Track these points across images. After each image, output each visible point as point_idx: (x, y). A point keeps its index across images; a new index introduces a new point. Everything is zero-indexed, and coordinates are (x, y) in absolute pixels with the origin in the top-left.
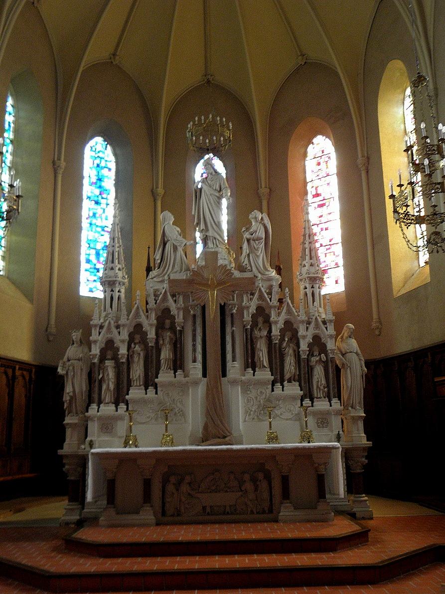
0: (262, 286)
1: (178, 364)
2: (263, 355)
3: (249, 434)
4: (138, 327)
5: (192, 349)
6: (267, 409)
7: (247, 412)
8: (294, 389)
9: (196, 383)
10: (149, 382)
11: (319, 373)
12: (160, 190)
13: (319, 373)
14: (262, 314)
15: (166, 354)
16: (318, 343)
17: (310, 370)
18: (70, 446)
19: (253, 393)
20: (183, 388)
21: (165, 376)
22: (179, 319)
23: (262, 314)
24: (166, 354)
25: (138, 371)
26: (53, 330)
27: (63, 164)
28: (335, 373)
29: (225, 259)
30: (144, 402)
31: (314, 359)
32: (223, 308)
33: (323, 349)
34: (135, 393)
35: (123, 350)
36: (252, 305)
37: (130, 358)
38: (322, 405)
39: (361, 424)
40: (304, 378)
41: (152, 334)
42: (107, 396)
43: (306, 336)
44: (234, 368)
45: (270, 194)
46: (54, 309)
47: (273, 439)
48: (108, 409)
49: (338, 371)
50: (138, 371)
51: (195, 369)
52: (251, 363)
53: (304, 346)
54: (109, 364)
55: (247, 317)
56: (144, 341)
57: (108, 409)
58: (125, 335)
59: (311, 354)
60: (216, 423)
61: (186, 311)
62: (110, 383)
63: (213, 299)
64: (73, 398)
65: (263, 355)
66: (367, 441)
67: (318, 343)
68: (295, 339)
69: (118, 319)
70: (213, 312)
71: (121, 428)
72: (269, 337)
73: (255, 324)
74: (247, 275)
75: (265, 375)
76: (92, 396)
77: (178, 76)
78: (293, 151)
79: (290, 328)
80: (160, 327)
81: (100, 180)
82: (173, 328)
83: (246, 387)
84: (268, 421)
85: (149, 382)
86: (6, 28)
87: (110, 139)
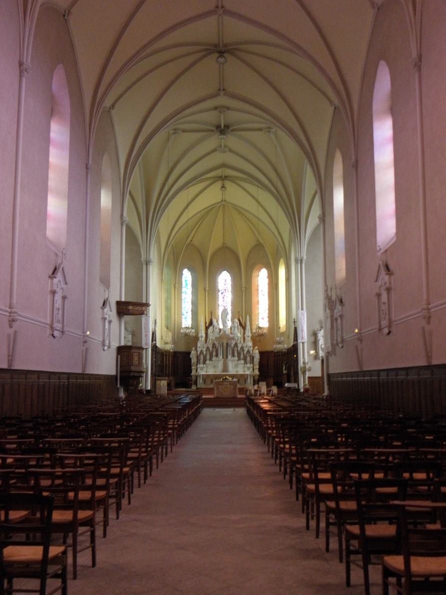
0: (236, 338)
1: (217, 355)
2: (236, 354)
3: (232, 370)
4: (208, 347)
5: (220, 352)
6: (236, 366)
7: (232, 366)
8: (242, 362)
9: (221, 360)
10: (211, 359)
11: (248, 358)
12: (207, 289)
13: (248, 358)
14: (236, 345)
15: (214, 353)
16: (248, 351)
17: (246, 357)
18: (193, 373)
19: (234, 362)
20: (218, 361)
21: (214, 358)
22: (217, 345)
23: (236, 345)
24: (214, 353)
25: (208, 357)
26: (176, 340)
27: (177, 286)
28: (252, 358)
29: (228, 332)
30: (209, 364)
31: (247, 355)
32: (227, 344)
33: (250, 353)
34: (208, 362)
35: (205, 353)
36: (234, 343)
37: (206, 354)
38: (249, 365)
39: (257, 370)
40: (245, 359)
41: (211, 349)
42: (202, 363)
43: (246, 350)
44: (229, 357)
45: (246, 290)
46: (176, 335)
47: (237, 372)
48: (201, 365)
49: (253, 358)
50: (208, 357)
51: (221, 357)
52: (233, 355)
53: (245, 352)
54: (202, 355)
55: (233, 345)
56: (209, 350)
57: (201, 365)
58: (205, 349)
59: (247, 354)
60: (225, 368)
61: (219, 343)
62: (202, 360)
63: (225, 342)
64: (194, 363)
65: (236, 354)
66: (309, 378)
67: (248, 351)
68: (243, 351)
69: (203, 346)
70: (225, 345)
71: (205, 369)
72: (237, 350)
73: (234, 347)
74: (233, 336)
75: (236, 358)
76: (198, 362)
77: (215, 243)
78: (254, 274)
79: (242, 348)
80: (213, 347)
81: (186, 285)
82: (216, 347)
83: (232, 361)
84: (237, 368)
85: (211, 359)
86: (34, 4)
87: (189, 269)
